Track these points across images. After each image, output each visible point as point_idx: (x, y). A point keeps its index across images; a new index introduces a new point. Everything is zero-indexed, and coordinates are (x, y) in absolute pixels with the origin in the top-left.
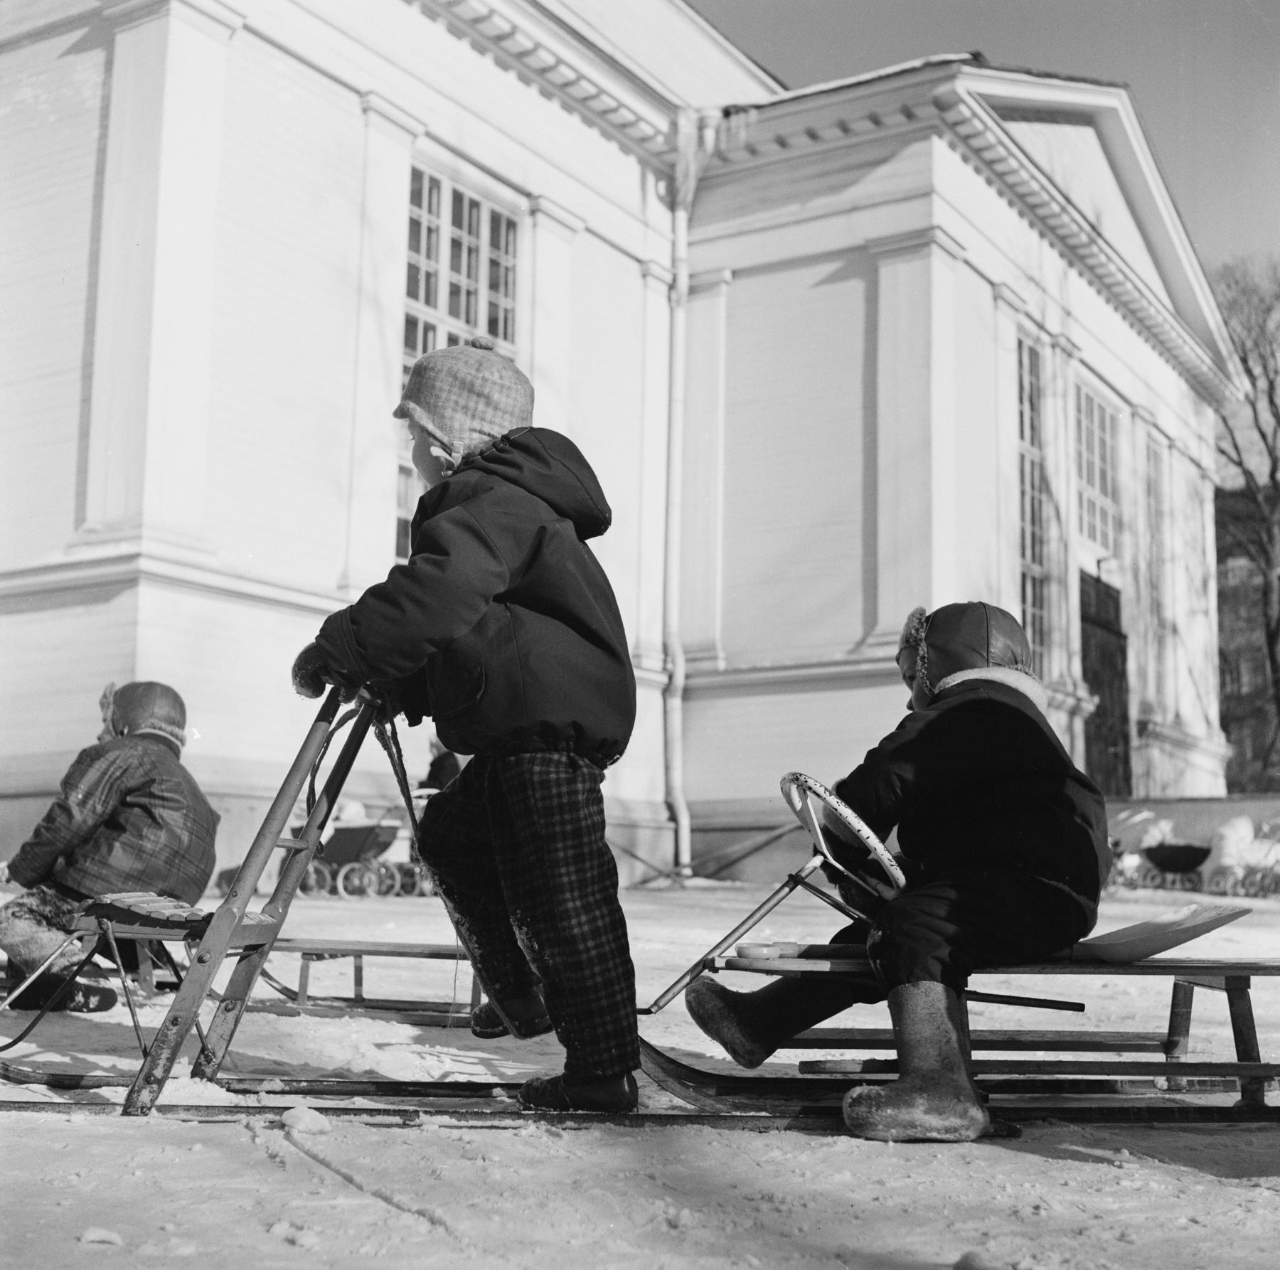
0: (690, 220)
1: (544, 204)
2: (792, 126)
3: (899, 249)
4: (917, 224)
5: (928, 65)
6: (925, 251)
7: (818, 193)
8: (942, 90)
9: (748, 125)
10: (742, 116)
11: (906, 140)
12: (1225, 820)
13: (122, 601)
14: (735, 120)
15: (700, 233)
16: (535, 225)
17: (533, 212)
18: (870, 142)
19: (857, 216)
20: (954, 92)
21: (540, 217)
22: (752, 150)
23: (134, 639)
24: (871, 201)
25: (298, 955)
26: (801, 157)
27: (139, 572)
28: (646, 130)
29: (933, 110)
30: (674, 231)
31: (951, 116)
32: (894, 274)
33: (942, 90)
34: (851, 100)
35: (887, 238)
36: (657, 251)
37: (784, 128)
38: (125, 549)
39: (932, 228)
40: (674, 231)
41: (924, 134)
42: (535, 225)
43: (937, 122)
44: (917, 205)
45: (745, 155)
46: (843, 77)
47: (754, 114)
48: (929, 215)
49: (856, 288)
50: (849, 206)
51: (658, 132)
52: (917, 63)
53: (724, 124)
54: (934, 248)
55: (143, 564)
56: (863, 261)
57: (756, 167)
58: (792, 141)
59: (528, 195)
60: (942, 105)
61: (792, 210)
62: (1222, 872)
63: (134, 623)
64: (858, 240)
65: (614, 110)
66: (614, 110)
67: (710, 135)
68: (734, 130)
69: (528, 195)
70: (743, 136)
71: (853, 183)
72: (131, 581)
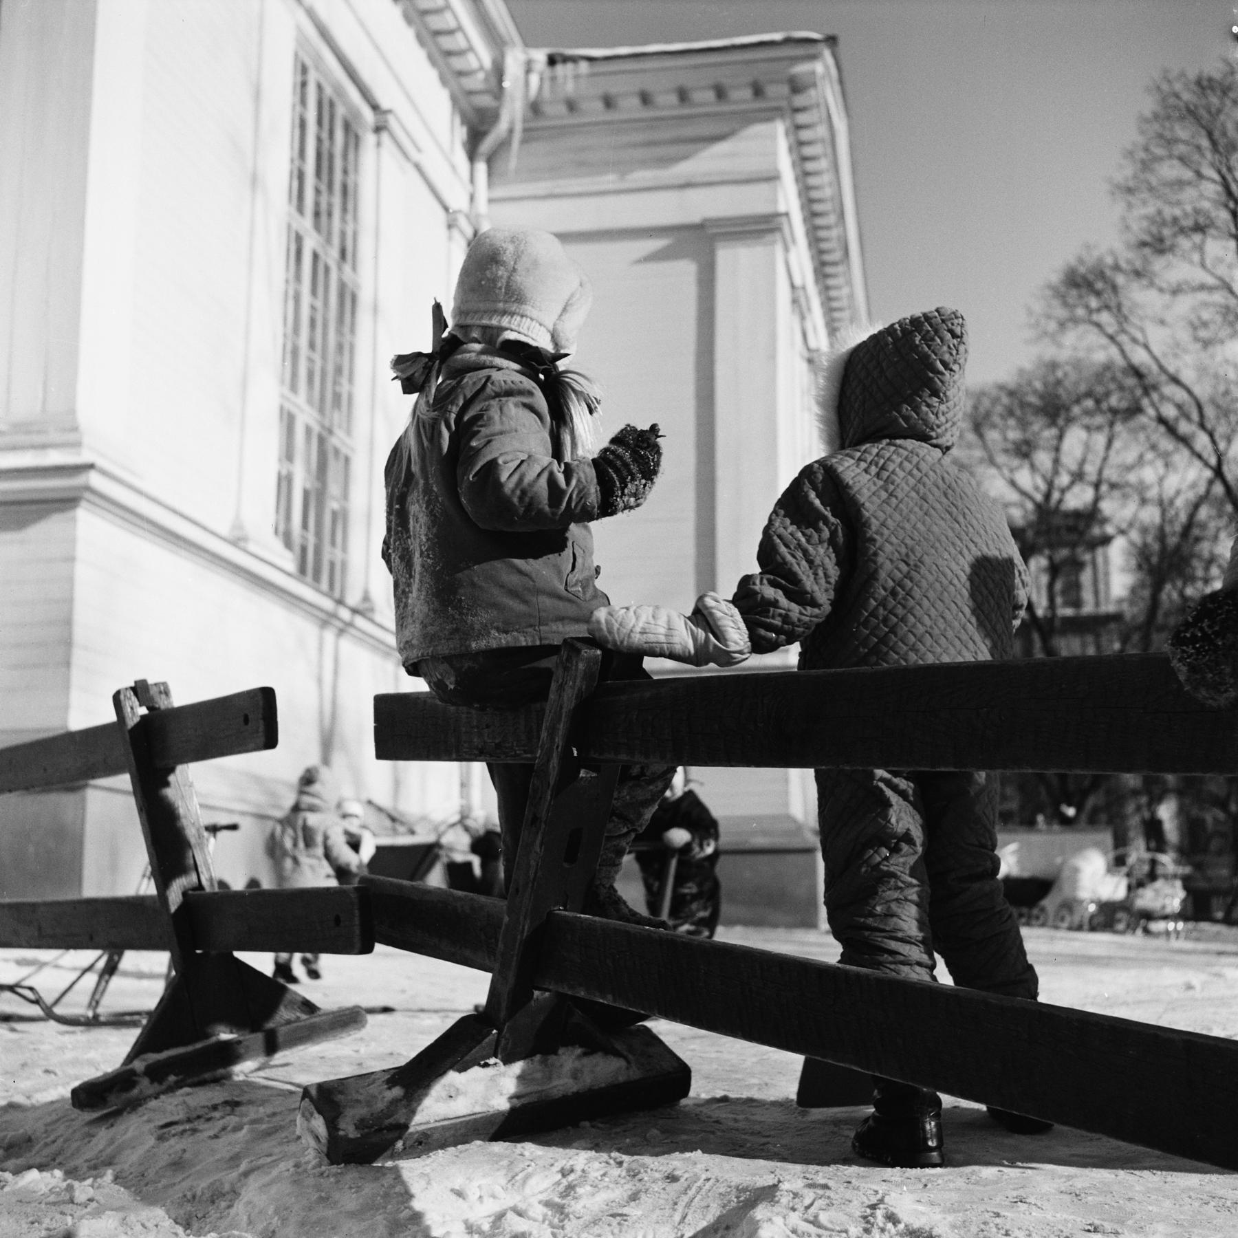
0: (490, 174)
1: (392, 122)
2: (624, 85)
3: (741, 233)
4: (761, 208)
5: (788, 41)
6: (769, 237)
7: (644, 164)
8: (800, 69)
9: (577, 77)
10: (570, 66)
11: (748, 118)
12: (1079, 849)
13: (49, 528)
14: (560, 69)
15: (500, 192)
16: (379, 144)
17: (378, 129)
18: (707, 115)
19: (691, 193)
20: (813, 73)
21: (385, 136)
22: (571, 106)
23: (70, 580)
24: (705, 179)
25: (102, 1019)
26: (626, 121)
27: (88, 488)
28: (471, 62)
29: (785, 89)
30: (472, 180)
31: (799, 101)
32: (734, 261)
33: (800, 69)
34: (696, 67)
35: (729, 219)
36: (458, 199)
37: (615, 86)
38: (55, 458)
39: (778, 215)
40: (472, 180)
41: (769, 115)
42: (379, 144)
43: (784, 104)
44: (763, 188)
45: (563, 109)
46: (667, 42)
47: (584, 67)
48: (775, 201)
49: (685, 271)
50: (682, 181)
51: (481, 68)
52: (777, 36)
53: (548, 72)
54: (778, 236)
55: (94, 479)
56: (699, 241)
57: (574, 126)
58: (584, 106)
59: (375, 107)
60: (796, 87)
61: (609, 180)
62: (1069, 905)
63: (71, 559)
64: (695, 218)
65: (450, 32)
66: (450, 32)
67: (534, 79)
68: (560, 80)
69: (375, 107)
70: (570, 87)
71: (685, 157)
72: (67, 502)
